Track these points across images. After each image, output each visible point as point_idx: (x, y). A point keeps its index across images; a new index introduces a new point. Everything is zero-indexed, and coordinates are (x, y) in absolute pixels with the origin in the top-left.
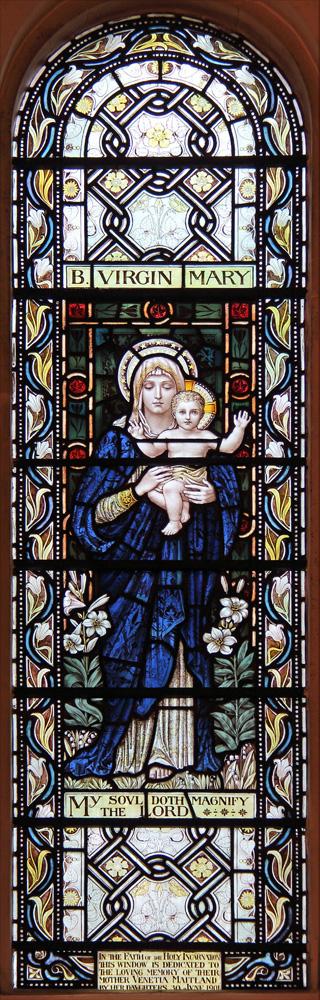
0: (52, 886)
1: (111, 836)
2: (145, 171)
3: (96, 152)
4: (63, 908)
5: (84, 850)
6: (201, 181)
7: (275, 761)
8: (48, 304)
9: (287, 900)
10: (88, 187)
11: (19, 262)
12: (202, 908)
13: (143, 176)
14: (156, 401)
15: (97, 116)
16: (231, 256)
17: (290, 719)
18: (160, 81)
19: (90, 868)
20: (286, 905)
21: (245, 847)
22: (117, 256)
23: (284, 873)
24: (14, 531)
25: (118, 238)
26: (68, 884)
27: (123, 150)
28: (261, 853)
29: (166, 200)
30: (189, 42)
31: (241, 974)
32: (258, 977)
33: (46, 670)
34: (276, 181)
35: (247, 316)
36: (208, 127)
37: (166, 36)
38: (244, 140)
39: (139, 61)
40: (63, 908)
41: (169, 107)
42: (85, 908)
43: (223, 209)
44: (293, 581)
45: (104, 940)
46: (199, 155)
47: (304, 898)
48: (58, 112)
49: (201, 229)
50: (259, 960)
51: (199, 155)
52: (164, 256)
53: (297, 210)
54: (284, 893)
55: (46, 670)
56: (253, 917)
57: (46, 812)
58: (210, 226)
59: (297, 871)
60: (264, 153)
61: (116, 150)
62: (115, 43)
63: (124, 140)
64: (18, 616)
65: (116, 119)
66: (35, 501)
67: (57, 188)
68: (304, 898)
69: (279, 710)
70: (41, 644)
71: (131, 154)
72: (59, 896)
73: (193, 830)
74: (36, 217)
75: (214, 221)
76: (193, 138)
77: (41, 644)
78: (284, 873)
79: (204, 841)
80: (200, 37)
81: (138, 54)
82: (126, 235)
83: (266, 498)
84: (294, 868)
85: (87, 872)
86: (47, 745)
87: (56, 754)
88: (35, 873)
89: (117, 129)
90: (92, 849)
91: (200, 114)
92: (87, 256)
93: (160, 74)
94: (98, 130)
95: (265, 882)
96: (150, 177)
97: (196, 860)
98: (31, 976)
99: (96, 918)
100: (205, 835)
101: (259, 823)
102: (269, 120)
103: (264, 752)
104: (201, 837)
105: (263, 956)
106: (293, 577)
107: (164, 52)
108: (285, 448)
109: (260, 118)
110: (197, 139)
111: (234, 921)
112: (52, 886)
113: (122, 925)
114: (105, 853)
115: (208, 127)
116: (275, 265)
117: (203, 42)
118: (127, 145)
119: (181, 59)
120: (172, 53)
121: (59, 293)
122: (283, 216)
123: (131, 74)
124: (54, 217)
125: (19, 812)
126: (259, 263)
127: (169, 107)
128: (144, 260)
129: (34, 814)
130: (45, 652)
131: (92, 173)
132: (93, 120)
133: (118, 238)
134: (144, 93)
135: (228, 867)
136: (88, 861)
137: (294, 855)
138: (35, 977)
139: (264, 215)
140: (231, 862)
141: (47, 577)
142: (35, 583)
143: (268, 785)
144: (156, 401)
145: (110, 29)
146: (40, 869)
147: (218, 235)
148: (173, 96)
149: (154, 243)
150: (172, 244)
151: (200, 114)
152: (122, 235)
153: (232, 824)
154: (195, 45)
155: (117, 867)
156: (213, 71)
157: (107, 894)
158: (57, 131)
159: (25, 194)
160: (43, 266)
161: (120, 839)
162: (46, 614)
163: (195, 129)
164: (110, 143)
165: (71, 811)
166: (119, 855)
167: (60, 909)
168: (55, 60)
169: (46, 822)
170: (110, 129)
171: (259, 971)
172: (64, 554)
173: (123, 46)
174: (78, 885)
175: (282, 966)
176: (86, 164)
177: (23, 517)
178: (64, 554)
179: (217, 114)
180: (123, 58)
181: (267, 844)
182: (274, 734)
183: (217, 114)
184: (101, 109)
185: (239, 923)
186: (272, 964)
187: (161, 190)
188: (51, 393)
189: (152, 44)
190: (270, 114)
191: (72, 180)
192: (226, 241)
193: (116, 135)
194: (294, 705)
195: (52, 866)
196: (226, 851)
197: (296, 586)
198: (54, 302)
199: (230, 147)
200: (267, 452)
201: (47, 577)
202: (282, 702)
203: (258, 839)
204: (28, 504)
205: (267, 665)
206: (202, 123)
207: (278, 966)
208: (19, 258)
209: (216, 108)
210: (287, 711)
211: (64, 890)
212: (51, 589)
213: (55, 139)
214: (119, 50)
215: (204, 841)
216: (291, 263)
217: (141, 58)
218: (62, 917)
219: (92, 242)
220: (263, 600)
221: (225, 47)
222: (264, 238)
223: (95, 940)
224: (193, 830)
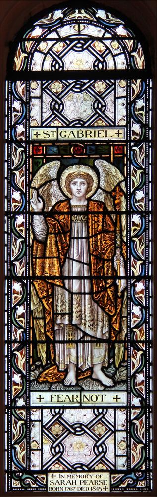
0: (25, 440)
1: (54, 414)
2: (70, 81)
4: (31, 450)
5: (41, 421)
6: (100, 86)
7: (136, 374)
8: (23, 147)
9: (143, 445)
10: (42, 90)
11: (8, 400)
12: (100, 449)
13: (70, 84)
14: (77, 191)
15: (48, 52)
16: (114, 123)
17: (144, 355)
18: (79, 34)
20: (142, 448)
21: (121, 417)
22: (57, 123)
23: (141, 432)
24: (6, 444)
25: (58, 115)
26: (32, 117)
28: (129, 422)
29: (81, 95)
30: (94, 14)
31: (119, 483)
32: (128, 484)
33: (22, 330)
34: (136, 87)
36: (104, 58)
37: (83, 11)
38: (121, 63)
39: (69, 24)
40: (31, 450)
42: (41, 450)
43: (109, 100)
44: (145, 285)
45: (50, 81)
48: (28, 51)
49: (99, 107)
50: (129, 476)
52: (80, 123)
54: (140, 259)
55: (22, 330)
56: (125, 454)
58: (103, 108)
59: (147, 431)
62: (58, 14)
63: (61, 65)
64: (8, 302)
65: (58, 54)
66: (16, 335)
67: (28, 90)
69: (139, 350)
70: (19, 317)
72: (28, 443)
74: (17, 105)
75: (105, 106)
76: (96, 64)
77: (19, 317)
78: (141, 432)
80: (99, 11)
81: (68, 21)
82: (62, 113)
83: (132, 59)
84: (146, 430)
85: (42, 431)
86: (22, 367)
87: (26, 372)
88: (16, 432)
91: (99, 51)
92: (42, 123)
93: (79, 31)
94: (49, 60)
95: (131, 436)
96: (74, 84)
97: (97, 465)
98: (15, 485)
99: (47, 456)
102: (133, 54)
103: (130, 371)
104: (100, 414)
105: (131, 474)
106: (145, 283)
107: (82, 20)
108: (141, 402)
109: (129, 53)
110: (98, 64)
111: (116, 456)
112: (25, 440)
114: (51, 119)
115: (104, 58)
116: (136, 128)
117: (101, 14)
119: (90, 23)
120: (86, 20)
122: (140, 103)
123: (66, 31)
124: (26, 105)
126: (128, 125)
128: (71, 125)
129: (15, 404)
130: (22, 413)
131: (45, 83)
132: (46, 55)
133: (58, 115)
134: (71, 50)
135: (113, 429)
136: (43, 427)
137: (146, 423)
138: (16, 485)
139: (130, 105)
140: (114, 427)
141: (23, 283)
142: (17, 287)
144: (77, 191)
146: (18, 158)
147: (107, 113)
149: (76, 117)
150: (85, 116)
151: (99, 51)
152: (60, 113)
153: (115, 408)
154: (97, 16)
155: (57, 429)
156: (107, 27)
158: (28, 60)
159: (11, 93)
160: (20, 129)
163: (97, 59)
164: (55, 66)
166: (57, 120)
167: (29, 451)
170: (55, 59)
171: (128, 481)
173: (62, 16)
174: (38, 438)
175: (140, 479)
177: (11, 436)
179: (108, 51)
180: (62, 23)
181: (132, 419)
182: (136, 362)
183: (108, 51)
184: (50, 49)
185: (118, 432)
186: (135, 478)
188: (25, 374)
189: (76, 15)
190: (134, 50)
191: (35, 441)
192: (111, 116)
193: (57, 62)
194: (146, 347)
196: (112, 421)
197: (147, 288)
198: (26, 145)
200: (132, 403)
201: (23, 283)
202: (140, 345)
203: (128, 414)
204: (13, 429)
205: (132, 327)
206: (101, 56)
207: (136, 481)
208: (8, 398)
209: (108, 48)
210: (142, 350)
211: (31, 441)
212: (25, 288)
213: (26, 388)
214: (60, 18)
216: (143, 126)
217: (70, 23)
218: (30, 454)
219: (45, 116)
221: (112, 16)
222: (131, 116)
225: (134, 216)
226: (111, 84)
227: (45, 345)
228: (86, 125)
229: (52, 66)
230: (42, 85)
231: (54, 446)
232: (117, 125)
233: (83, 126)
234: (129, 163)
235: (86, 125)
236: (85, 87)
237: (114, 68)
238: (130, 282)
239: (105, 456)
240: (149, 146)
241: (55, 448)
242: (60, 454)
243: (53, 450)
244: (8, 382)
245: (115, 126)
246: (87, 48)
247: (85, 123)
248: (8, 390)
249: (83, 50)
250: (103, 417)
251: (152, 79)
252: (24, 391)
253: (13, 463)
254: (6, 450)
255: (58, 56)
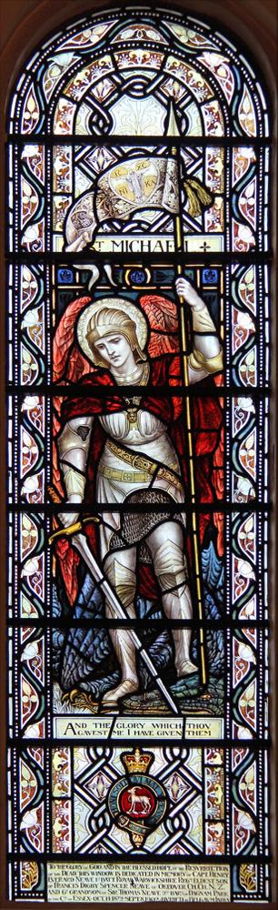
3: (83, 129)
15: (83, 99)
16: (202, 227)
19: (76, 787)
27: (106, 130)
35: (216, 281)
41: (148, 91)
46: (99, 134)
47: (266, 574)
51: (99, 134)
53: (261, 183)
57: (33, 732)
60: (231, 134)
61: (101, 130)
68: (266, 574)
71: (114, 132)
73: (168, 750)
79: (178, 762)
89: (101, 116)
90: (78, 771)
94: (85, 112)
100: (104, 755)
101: (228, 744)
113: (105, 840)
118: (110, 126)
121: (49, 258)
125: (14, 733)
127: (148, 91)
132: (79, 105)
143: (234, 377)
145: (91, 23)
148: (151, 82)
157: (92, 810)
161: (103, 760)
162: (37, 801)
164: (96, 124)
165: (61, 729)
168: (47, 48)
169: (34, 743)
170: (96, 111)
172: (54, 572)
176: (73, 140)
178: (54, 572)
183: (189, 98)
187: (141, 94)
193: (101, 117)
195: (43, 203)
199: (199, 119)
215: (178, 762)
220: (230, 292)
223: (83, 851)
224: (168, 750)
225: (239, 399)
226: (196, 156)
227: (64, 515)
228: (153, 230)
229: (91, 124)
230: (75, 155)
231: (96, 815)
232: (206, 231)
233: (147, 232)
234: (230, 706)
235: (153, 230)
236: (152, 87)
237: (201, 135)
238: (230, 270)
239: (186, 835)
240: (264, 638)
241: (97, 820)
242: (105, 830)
243: (93, 822)
244: (12, 786)
245: (204, 233)
246: (152, 93)
247: (151, 226)
248: (13, 287)
249: (146, 95)
250: (181, 765)
251: (269, 398)
252: (41, 126)
253: (22, 344)
254: (10, 418)
255: (101, 105)
